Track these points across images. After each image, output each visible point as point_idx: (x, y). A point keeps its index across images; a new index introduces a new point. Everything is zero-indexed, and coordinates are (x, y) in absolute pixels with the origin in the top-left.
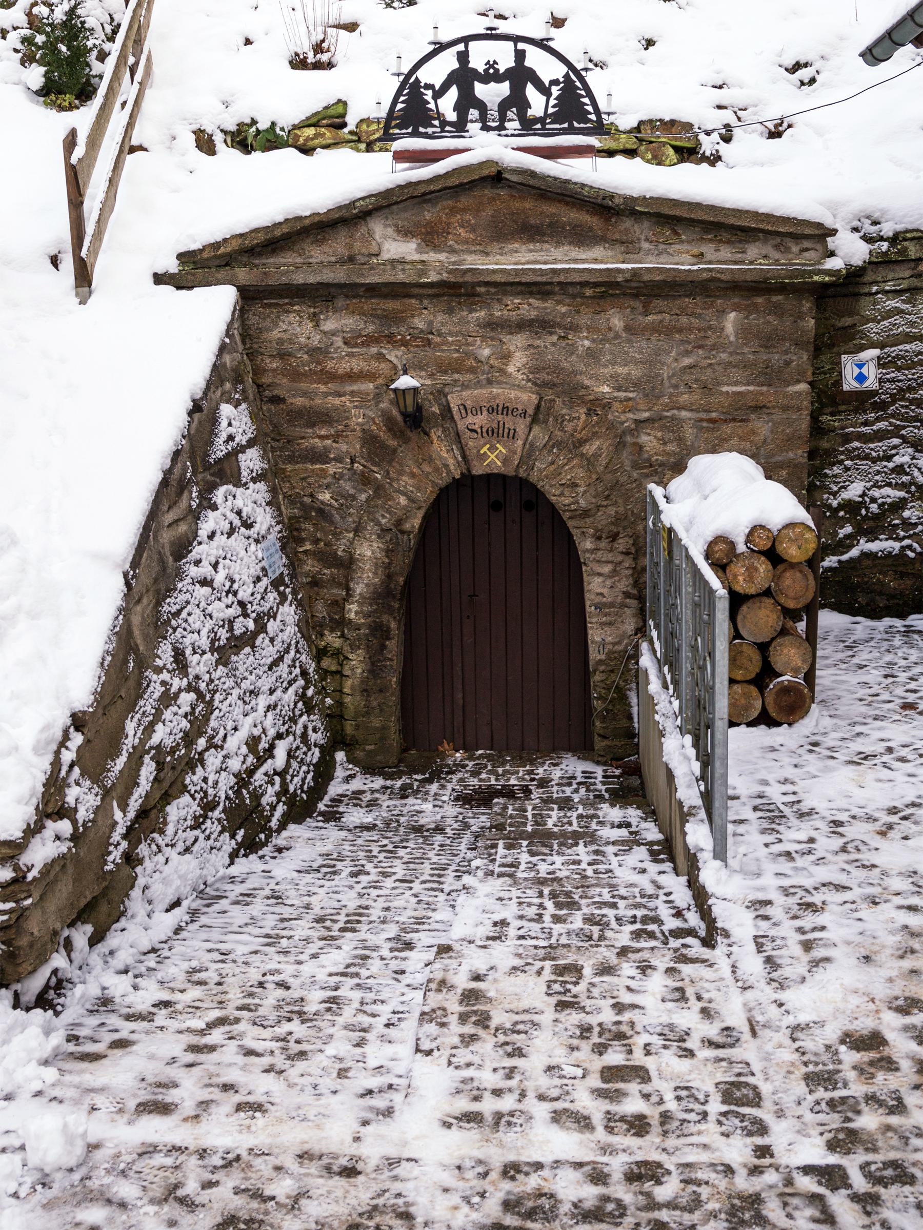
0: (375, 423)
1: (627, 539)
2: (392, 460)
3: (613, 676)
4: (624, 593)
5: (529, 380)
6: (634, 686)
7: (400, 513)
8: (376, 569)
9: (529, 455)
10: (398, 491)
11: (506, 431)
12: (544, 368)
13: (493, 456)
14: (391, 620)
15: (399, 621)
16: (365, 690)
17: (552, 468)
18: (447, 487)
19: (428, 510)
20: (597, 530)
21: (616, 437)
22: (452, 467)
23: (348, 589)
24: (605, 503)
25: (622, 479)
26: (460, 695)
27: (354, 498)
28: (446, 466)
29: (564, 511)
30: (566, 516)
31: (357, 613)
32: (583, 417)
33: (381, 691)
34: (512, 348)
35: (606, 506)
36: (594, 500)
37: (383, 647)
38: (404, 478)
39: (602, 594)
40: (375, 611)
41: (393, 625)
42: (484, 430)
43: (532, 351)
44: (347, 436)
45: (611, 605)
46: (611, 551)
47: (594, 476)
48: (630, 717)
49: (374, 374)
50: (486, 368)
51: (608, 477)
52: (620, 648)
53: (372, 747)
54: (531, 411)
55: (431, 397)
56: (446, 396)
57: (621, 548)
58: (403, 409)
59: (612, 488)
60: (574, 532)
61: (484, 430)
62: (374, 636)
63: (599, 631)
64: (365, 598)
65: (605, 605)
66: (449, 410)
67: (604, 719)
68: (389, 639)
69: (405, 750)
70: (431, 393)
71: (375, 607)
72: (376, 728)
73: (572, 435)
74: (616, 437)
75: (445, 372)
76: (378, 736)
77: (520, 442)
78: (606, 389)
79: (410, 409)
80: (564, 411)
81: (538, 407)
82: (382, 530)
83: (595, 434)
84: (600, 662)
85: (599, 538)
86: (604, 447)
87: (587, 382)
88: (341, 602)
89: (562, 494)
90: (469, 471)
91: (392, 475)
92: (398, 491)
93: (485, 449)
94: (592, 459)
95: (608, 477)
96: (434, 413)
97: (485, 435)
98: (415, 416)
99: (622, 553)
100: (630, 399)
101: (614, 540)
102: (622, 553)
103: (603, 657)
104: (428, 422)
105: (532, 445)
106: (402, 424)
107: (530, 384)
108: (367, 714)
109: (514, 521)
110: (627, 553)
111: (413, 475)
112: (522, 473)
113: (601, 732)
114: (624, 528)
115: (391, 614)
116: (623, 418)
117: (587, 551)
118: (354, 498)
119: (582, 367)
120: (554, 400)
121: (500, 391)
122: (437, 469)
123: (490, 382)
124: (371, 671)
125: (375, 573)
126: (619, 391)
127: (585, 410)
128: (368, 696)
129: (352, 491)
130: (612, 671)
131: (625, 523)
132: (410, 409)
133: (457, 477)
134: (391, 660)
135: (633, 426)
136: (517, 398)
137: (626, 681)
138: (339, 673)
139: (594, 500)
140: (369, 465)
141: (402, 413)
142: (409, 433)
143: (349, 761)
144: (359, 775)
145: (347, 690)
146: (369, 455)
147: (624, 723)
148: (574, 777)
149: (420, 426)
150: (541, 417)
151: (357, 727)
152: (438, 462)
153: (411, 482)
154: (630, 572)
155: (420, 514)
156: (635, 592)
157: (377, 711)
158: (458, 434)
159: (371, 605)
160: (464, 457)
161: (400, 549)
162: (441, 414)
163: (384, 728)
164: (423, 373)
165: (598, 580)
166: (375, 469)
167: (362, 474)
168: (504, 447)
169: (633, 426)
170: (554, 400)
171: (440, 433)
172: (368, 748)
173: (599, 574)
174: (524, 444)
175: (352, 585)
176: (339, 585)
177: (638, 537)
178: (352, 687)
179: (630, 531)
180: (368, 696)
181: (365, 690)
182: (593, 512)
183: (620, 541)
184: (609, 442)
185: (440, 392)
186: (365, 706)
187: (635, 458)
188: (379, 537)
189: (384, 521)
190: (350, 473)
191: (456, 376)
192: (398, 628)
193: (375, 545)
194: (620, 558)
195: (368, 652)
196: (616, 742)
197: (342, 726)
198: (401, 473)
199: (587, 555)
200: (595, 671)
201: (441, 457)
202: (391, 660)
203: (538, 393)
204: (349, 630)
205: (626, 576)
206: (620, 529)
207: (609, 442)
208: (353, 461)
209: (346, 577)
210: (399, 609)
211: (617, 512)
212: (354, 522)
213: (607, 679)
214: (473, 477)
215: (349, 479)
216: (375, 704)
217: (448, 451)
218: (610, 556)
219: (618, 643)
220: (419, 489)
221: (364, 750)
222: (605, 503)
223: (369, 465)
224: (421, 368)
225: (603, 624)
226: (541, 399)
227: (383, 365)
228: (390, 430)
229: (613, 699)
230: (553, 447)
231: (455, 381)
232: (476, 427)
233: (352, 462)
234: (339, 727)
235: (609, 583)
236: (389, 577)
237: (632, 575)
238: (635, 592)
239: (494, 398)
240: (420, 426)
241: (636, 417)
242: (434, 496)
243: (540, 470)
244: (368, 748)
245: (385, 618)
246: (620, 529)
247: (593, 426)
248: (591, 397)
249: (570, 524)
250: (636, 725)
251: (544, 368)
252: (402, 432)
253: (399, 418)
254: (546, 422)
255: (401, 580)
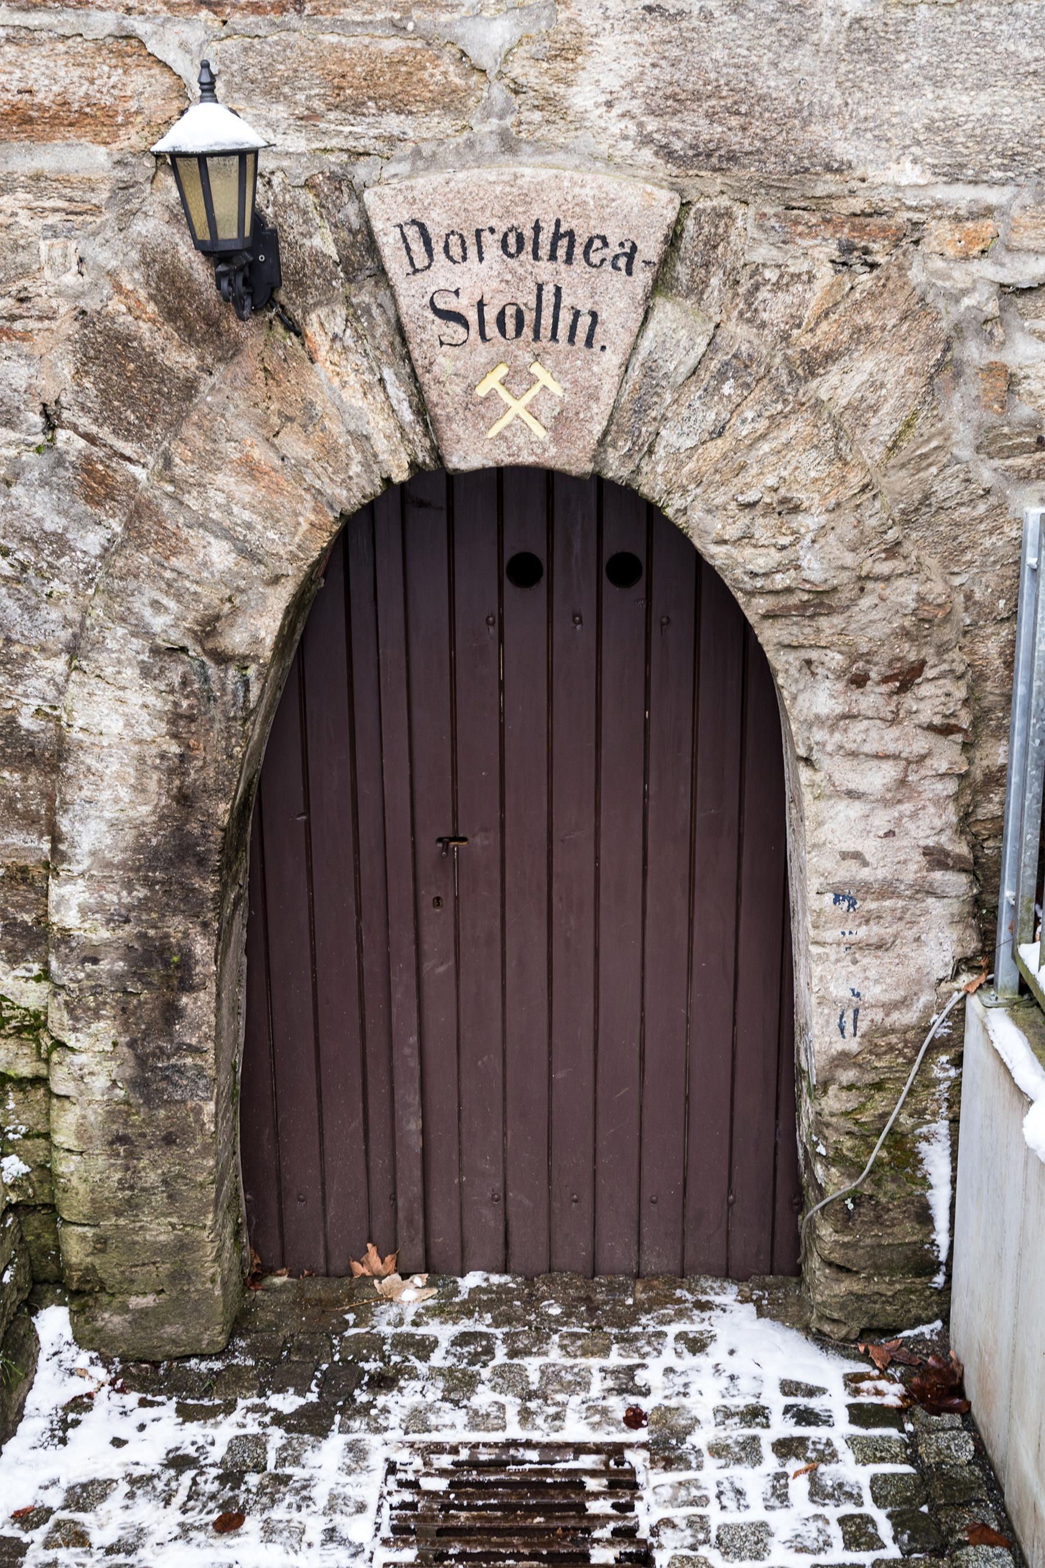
0: (118, 288)
1: (947, 684)
2: (182, 417)
3: (880, 1102)
4: (927, 852)
5: (646, 140)
6: (942, 1127)
7: (211, 596)
8: (141, 774)
9: (641, 408)
10: (203, 524)
11: (566, 317)
12: (697, 97)
13: (518, 407)
14: (195, 931)
15: (222, 938)
16: (122, 1139)
17: (716, 448)
18: (370, 509)
19: (309, 580)
20: (854, 657)
21: (930, 344)
22: (381, 445)
23: (56, 838)
24: (884, 568)
25: (946, 488)
26: (414, 1125)
27: (61, 544)
28: (362, 439)
29: (751, 594)
30: (754, 609)
31: (84, 911)
32: (825, 274)
33: (169, 1140)
34: (590, 19)
35: (887, 579)
36: (849, 559)
37: (171, 1013)
38: (221, 479)
39: (857, 856)
40: (143, 905)
41: (202, 947)
42: (491, 314)
43: (661, 29)
44: (25, 336)
45: (887, 890)
46: (894, 720)
47: (856, 479)
48: (924, 1216)
49: (110, 113)
50: (498, 92)
51: (900, 480)
52: (908, 1017)
53: (148, 1301)
54: (651, 249)
55: (308, 199)
56: (357, 196)
57: (928, 713)
58: (203, 234)
59: (907, 519)
60: (778, 660)
61: (491, 314)
62: (140, 977)
63: (846, 968)
64: (109, 865)
65: (866, 888)
66: (372, 247)
67: (845, 1220)
68: (190, 988)
69: (255, 1278)
70: (309, 185)
71: (141, 892)
72: (160, 1249)
73: (785, 337)
74: (930, 344)
75: (356, 108)
76: (165, 1268)
77: (612, 360)
78: (909, 174)
79: (228, 232)
80: (762, 253)
81: (673, 239)
82: (155, 651)
83: (861, 333)
84: (843, 1059)
85: (859, 681)
86: (890, 379)
87: (843, 150)
88: (37, 872)
89: (746, 537)
90: (439, 459)
91: (181, 469)
92: (203, 524)
93: (492, 382)
94: (847, 421)
95: (900, 480)
96: (317, 257)
97: (492, 330)
98: (253, 266)
99: (931, 728)
100: (988, 211)
101: (905, 687)
102: (931, 728)
103: (853, 1045)
104: (300, 285)
105: (649, 371)
106: (211, 293)
107: (647, 154)
108: (131, 1206)
109: (577, 617)
110: (945, 730)
111: (251, 470)
112: (616, 469)
113: (836, 1257)
114: (942, 649)
115: (194, 914)
116: (960, 276)
117: (819, 721)
118: (61, 544)
119: (831, 95)
120: (727, 214)
121: (544, 174)
122: (330, 451)
123: (508, 144)
124: (139, 1084)
125: (139, 789)
126: (953, 180)
127: (832, 249)
128: (131, 1155)
129: (53, 523)
130: (878, 1086)
131: (948, 633)
132: (228, 232)
133: (400, 476)
134: (196, 1050)
135: (992, 308)
136: (604, 202)
137: (920, 1113)
138: (39, 1081)
139: (849, 559)
140: (105, 433)
141: (199, 245)
142: (233, 323)
143: (80, 1340)
144: (106, 1403)
145: (64, 1138)
146: (106, 403)
147: (907, 1232)
148: (755, 1414)
149: (271, 302)
150: (682, 271)
151: (101, 1244)
152: (335, 428)
153: (244, 491)
154: (951, 787)
155: (280, 598)
156: (962, 849)
157: (159, 1199)
158: (400, 329)
159: (129, 886)
160: (422, 409)
161: (216, 712)
162: (345, 262)
163: (183, 1247)
164: (279, 111)
165: (849, 811)
166: (128, 448)
167: (86, 466)
168: (559, 374)
169: (992, 308)
170: (727, 214)
171: (337, 325)
172: (136, 1302)
173: (853, 795)
174: (626, 366)
175: (64, 824)
176: (29, 820)
177: (980, 677)
178: (82, 1132)
179: (957, 659)
180: (131, 1155)
181: (122, 1139)
182: (845, 595)
183: (926, 690)
184: (910, 360)
185: (339, 180)
186: (122, 1185)
187: (991, 418)
188: (146, 672)
189: (158, 623)
190: (45, 461)
191: (393, 123)
192: (220, 956)
193: (134, 698)
194: (922, 743)
195: (126, 1027)
196: (881, 1285)
197: (57, 1237)
198: (210, 461)
199: (819, 735)
200: (825, 1085)
201: (341, 410)
202: (196, 1050)
203: (673, 187)
204: (64, 961)
205: (937, 802)
206: (929, 653)
207: (910, 360)
208: (51, 423)
209: (49, 797)
210: (220, 897)
211: (921, 598)
212: (67, 623)
213: (861, 1108)
214: (453, 479)
215: (44, 483)
216: (152, 1177)
217: (366, 389)
218: (889, 739)
219: (903, 1003)
220: (271, 517)
221: (124, 1309)
222: (884, 568)
223: (105, 433)
224: (273, 92)
225: (856, 948)
226: (686, 205)
227: (138, 80)
228: (172, 314)
229: (879, 1163)
230: (721, 376)
231: (392, 140)
232: (464, 305)
233: (51, 424)
234: (47, 1238)
235: (882, 820)
236: (184, 799)
237: (956, 797)
238: (962, 849)
239: (525, 199)
240: (271, 302)
241: (1006, 276)
242: (323, 540)
243: (677, 459)
244: (136, 1302)
245: (176, 926)
246: (929, 653)
247: (858, 306)
248: (857, 204)
249: (768, 635)
250: (942, 1238)
251: (697, 97)
252: (212, 322)
253: (201, 272)
254: (697, 290)
255: (222, 810)
